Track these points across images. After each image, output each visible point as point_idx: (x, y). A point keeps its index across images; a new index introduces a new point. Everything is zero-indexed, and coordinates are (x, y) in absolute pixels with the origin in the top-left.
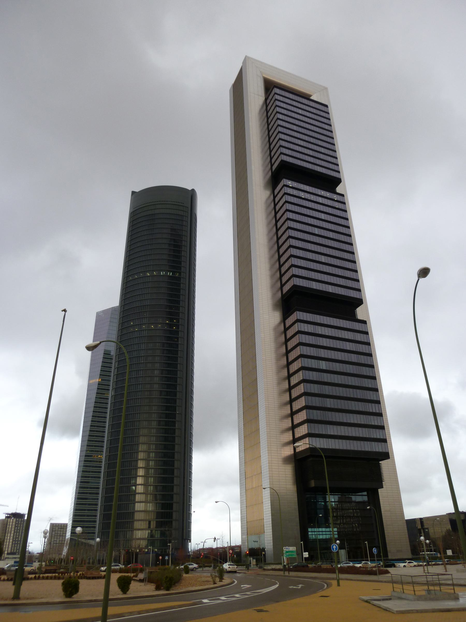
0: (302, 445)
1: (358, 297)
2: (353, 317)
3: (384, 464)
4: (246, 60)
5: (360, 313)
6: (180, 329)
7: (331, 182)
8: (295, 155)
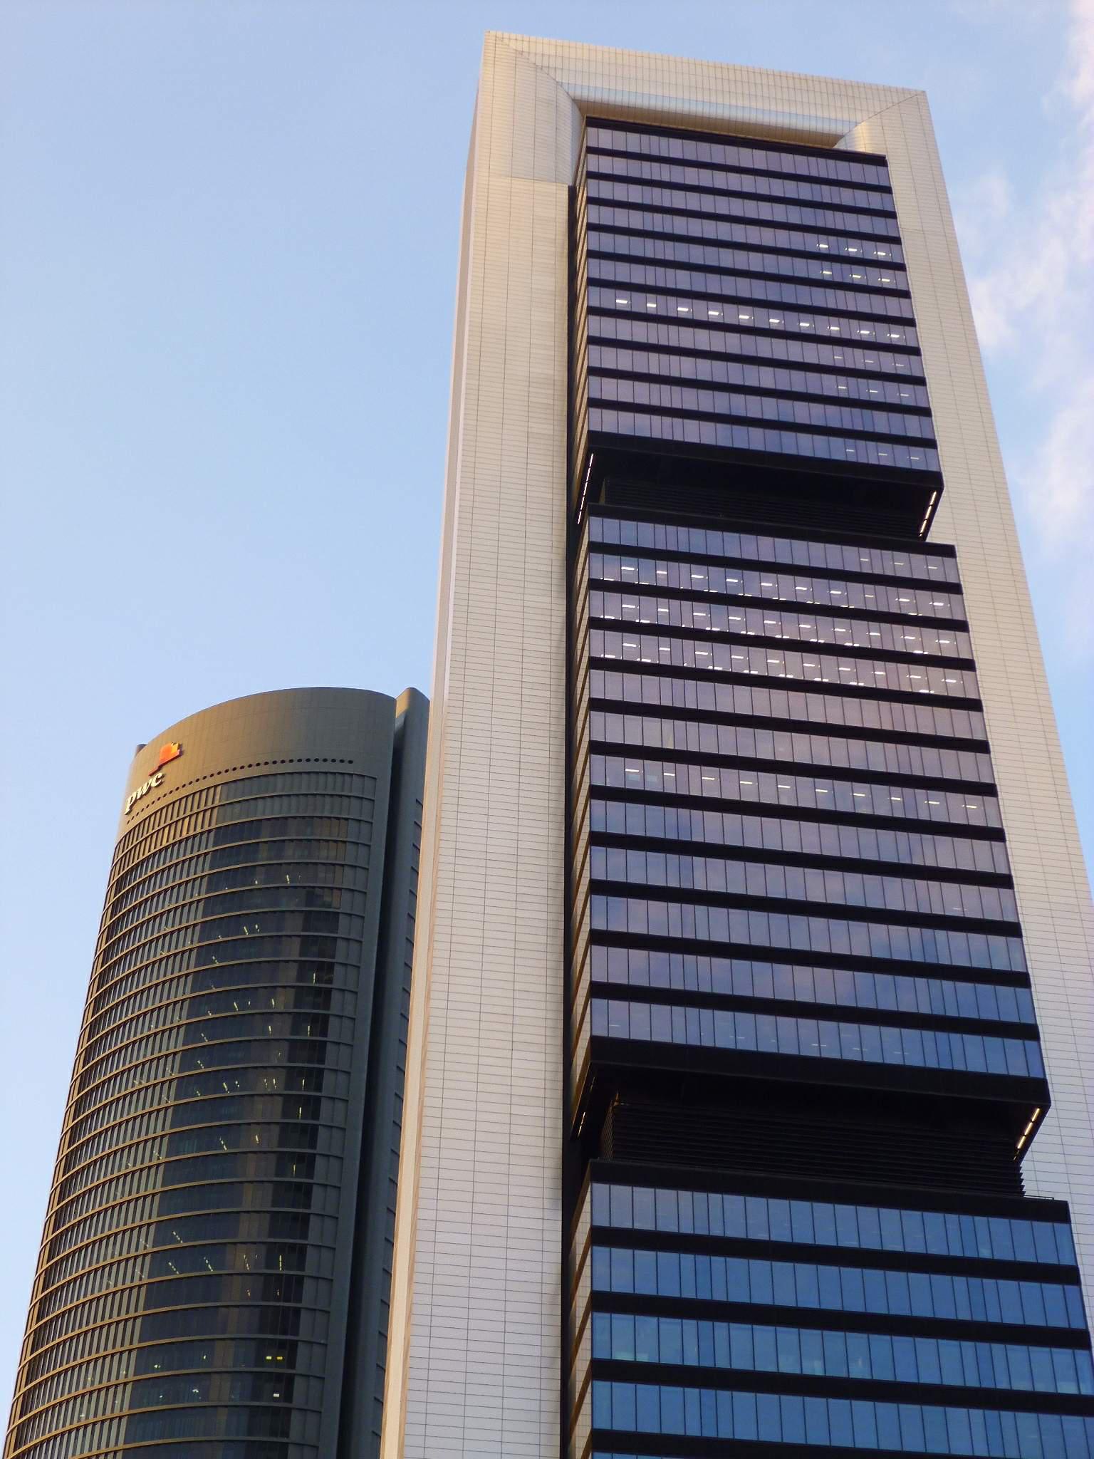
5: (1040, 1174)
7: (886, 503)
8: (745, 416)
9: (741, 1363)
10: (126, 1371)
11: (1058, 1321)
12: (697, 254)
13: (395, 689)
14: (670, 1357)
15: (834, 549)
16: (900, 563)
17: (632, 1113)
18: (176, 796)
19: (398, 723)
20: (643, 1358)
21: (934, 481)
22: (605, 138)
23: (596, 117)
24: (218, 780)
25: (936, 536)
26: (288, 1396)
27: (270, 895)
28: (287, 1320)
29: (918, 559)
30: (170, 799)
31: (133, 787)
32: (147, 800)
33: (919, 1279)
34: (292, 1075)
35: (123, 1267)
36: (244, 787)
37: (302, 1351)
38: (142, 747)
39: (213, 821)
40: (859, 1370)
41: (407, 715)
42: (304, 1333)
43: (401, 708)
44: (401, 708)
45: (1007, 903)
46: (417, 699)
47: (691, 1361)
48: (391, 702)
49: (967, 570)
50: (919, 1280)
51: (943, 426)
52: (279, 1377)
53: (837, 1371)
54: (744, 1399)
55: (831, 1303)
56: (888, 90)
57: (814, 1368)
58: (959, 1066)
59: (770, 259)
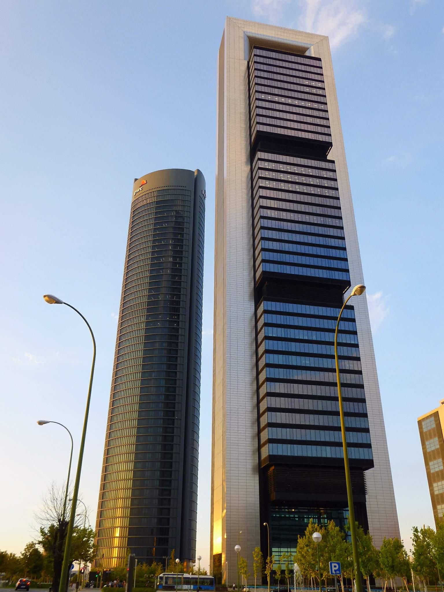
0: (265, 452)
3: (368, 473)
5: (349, 296)
6: (180, 326)
7: (319, 150)
8: (288, 122)
9: (293, 337)
10: (143, 319)
11: (351, 329)
12: (279, 84)
13: (194, 169)
14: (279, 335)
15: (306, 160)
16: (323, 165)
17: (269, 287)
18: (146, 193)
19: (195, 177)
20: (274, 336)
21: (330, 144)
22: (258, 52)
23: (255, 44)
24: (156, 190)
25: (329, 158)
26: (178, 325)
27: (169, 218)
28: (177, 310)
29: (327, 164)
30: (144, 193)
31: (135, 189)
32: (139, 193)
33: (325, 321)
34: (175, 258)
35: (142, 297)
36: (162, 192)
37: (180, 316)
38: (136, 180)
39: (155, 199)
40: (314, 338)
41: (197, 175)
42: (181, 313)
43: (196, 174)
44: (196, 174)
45: (344, 243)
46: (198, 171)
47: (283, 336)
48: (194, 172)
49: (337, 166)
50: (326, 321)
51: (333, 131)
52: (176, 321)
53: (310, 338)
54: (293, 344)
55: (309, 325)
56: (320, 36)
57: (306, 338)
58: (334, 278)
59: (262, 59)
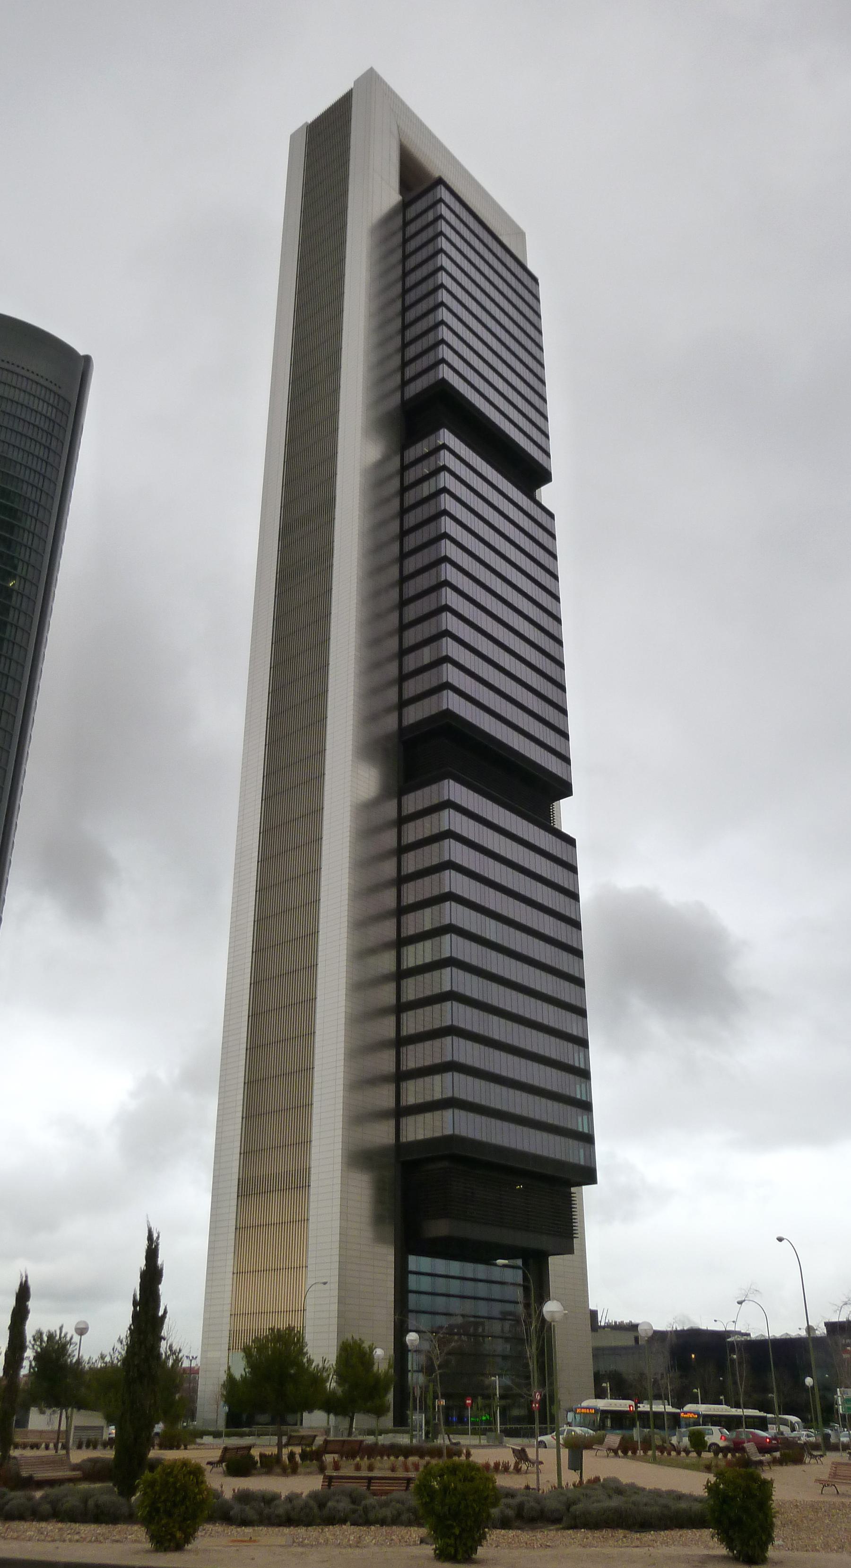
1: (565, 777)
2: (544, 819)
4: (370, 78)
46: (87, 359)
